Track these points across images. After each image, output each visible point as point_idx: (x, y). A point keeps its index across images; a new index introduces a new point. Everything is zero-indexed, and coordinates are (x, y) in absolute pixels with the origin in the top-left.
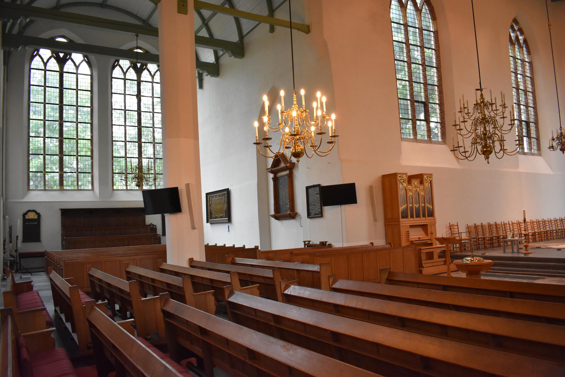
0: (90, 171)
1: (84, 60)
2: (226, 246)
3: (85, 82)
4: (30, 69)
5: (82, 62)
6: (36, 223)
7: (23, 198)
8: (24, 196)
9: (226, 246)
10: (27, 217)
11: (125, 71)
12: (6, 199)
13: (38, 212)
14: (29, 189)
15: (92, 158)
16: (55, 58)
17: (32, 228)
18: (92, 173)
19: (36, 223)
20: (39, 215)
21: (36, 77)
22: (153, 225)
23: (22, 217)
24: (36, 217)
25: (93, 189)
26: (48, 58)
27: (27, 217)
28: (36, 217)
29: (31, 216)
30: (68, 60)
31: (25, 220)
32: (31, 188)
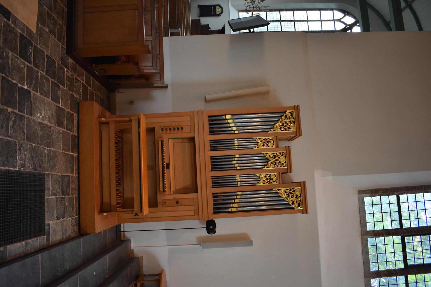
3: (328, 27)
5: (345, 24)
7: (232, 5)
13: (222, 15)
14: (239, 11)
21: (327, 15)
23: (217, 4)
24: (218, 13)
27: (217, 7)
28: (218, 13)
29: (219, 10)
31: (215, 6)
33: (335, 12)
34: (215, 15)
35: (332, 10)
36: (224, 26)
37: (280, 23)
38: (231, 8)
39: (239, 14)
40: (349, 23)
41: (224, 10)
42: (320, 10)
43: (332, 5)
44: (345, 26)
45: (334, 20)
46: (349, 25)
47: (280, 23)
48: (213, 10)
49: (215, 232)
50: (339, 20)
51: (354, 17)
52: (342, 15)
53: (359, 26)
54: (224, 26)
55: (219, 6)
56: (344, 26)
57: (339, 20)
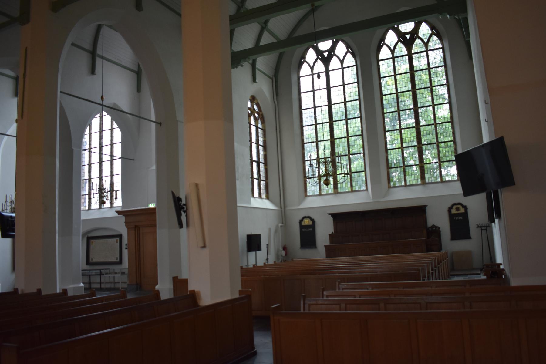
0: (363, 170)
1: (348, 51)
2: (44, 293)
3: (351, 75)
4: (378, 61)
5: (316, 61)
6: (311, 229)
7: (299, 204)
8: (300, 203)
9: (44, 293)
10: (303, 224)
11: (392, 48)
12: (285, 207)
13: (313, 217)
14: (306, 196)
15: (455, 143)
16: (402, 42)
17: (308, 235)
18: (365, 171)
19: (311, 229)
20: (313, 221)
21: (305, 84)
22: (436, 227)
23: (298, 224)
24: (311, 223)
25: (367, 189)
26: (394, 44)
27: (303, 224)
28: (311, 223)
29: (307, 222)
30: (303, 63)
31: (302, 227)
32: (308, 194)
33: (301, 75)
34: (465, 215)
35: (299, 78)
36: (329, 214)
37: (319, 143)
38: (303, 206)
39: (310, 196)
40: (315, 57)
41: (307, 215)
42: (300, 93)
43: (294, 78)
44: (349, 54)
45: (342, 68)
46: (399, 38)
47: (319, 143)
48: (306, 230)
49: (441, 249)
50: (342, 62)
51: (307, 50)
52: (418, 41)
53: (317, 44)
54: (329, 214)
55: (450, 209)
56: (349, 55)
57: (342, 62)
